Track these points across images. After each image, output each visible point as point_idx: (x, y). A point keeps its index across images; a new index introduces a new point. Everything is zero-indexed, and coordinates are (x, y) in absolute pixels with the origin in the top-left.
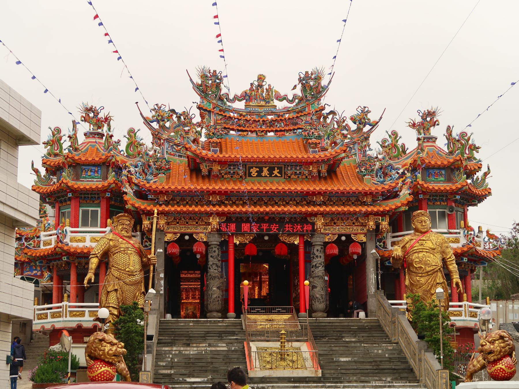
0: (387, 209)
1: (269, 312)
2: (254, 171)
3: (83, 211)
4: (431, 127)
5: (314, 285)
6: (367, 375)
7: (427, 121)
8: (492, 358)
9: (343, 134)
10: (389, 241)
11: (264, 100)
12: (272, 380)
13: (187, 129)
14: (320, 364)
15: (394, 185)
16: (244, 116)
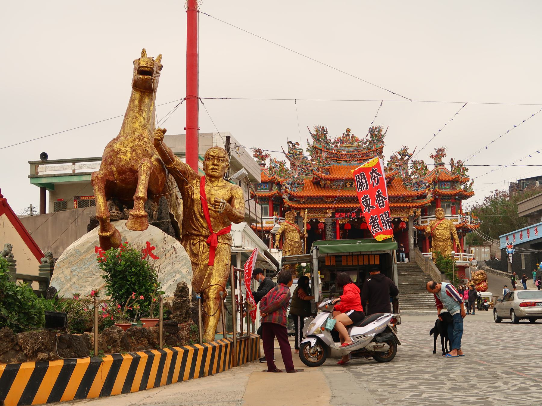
2: (348, 184)
6: (417, 290)
7: (439, 154)
8: (477, 282)
11: (350, 143)
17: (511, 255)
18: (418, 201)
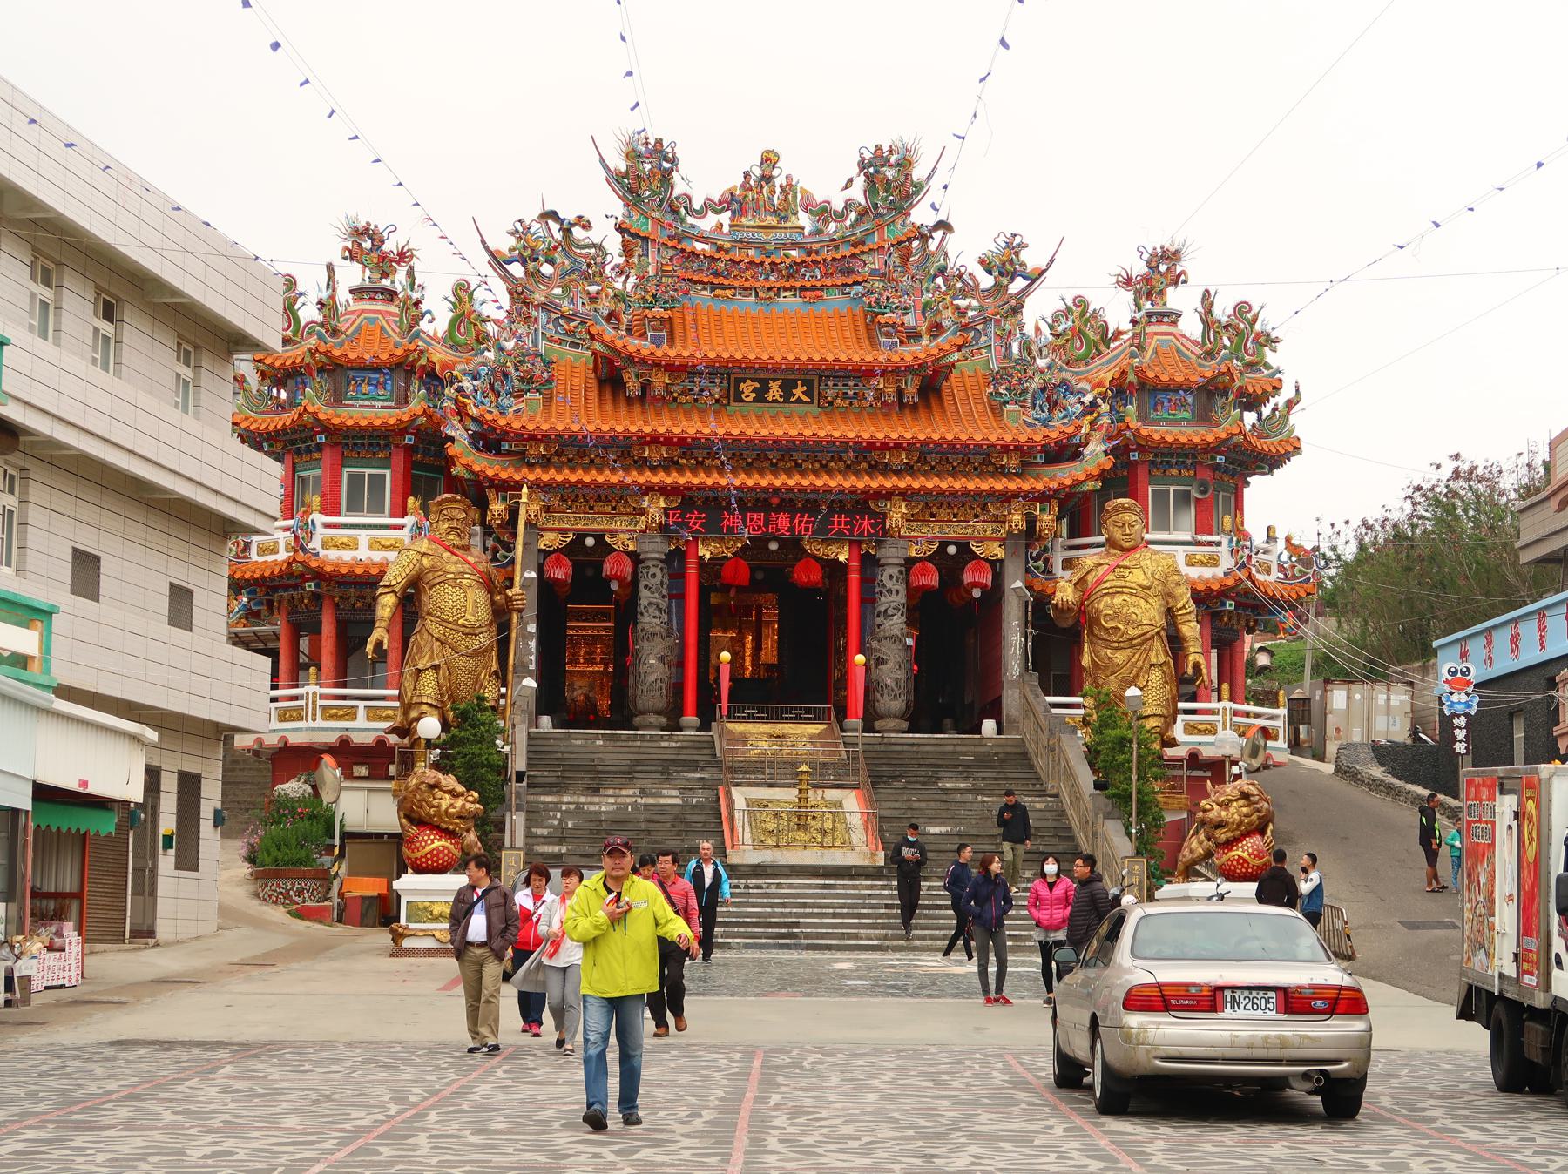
0: (1054, 485)
1: (774, 716)
2: (748, 389)
3: (350, 476)
4: (1167, 286)
5: (882, 656)
7: (1159, 274)
8: (1222, 835)
9: (958, 308)
10: (1058, 559)
11: (775, 212)
12: (1227, 665)
13: (593, 289)
15: (1070, 430)
16: (727, 252)
17: (1462, 721)
18: (1051, 470)
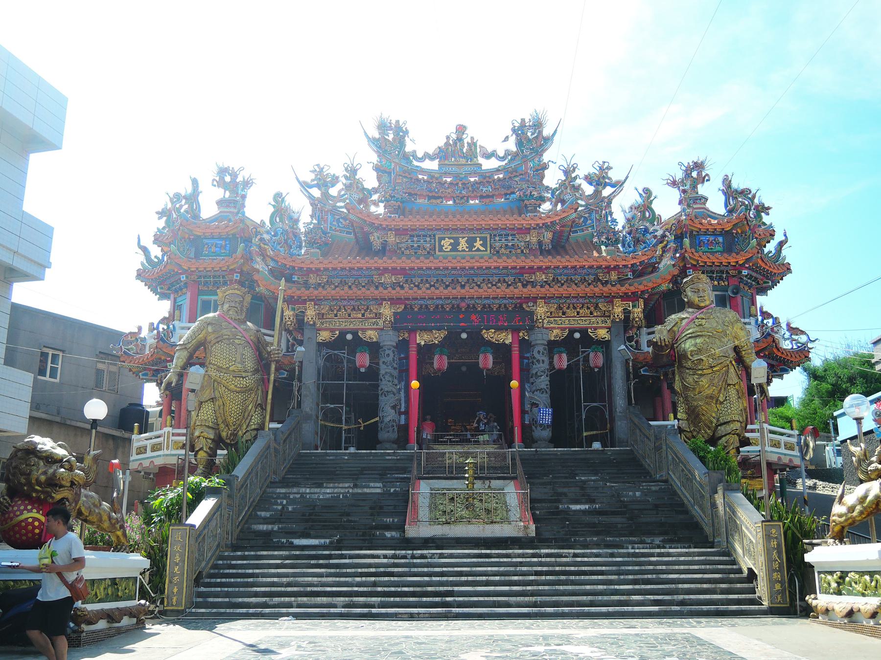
7: (693, 176)
11: (464, 157)
14: (533, 515)
16: (437, 179)
